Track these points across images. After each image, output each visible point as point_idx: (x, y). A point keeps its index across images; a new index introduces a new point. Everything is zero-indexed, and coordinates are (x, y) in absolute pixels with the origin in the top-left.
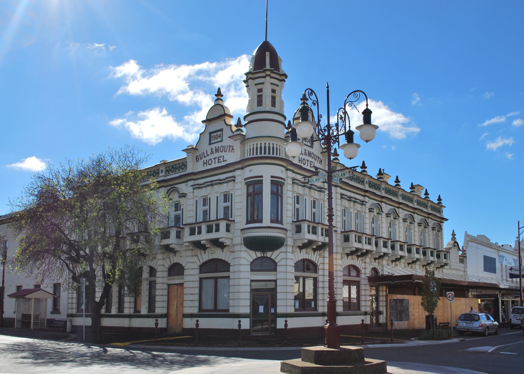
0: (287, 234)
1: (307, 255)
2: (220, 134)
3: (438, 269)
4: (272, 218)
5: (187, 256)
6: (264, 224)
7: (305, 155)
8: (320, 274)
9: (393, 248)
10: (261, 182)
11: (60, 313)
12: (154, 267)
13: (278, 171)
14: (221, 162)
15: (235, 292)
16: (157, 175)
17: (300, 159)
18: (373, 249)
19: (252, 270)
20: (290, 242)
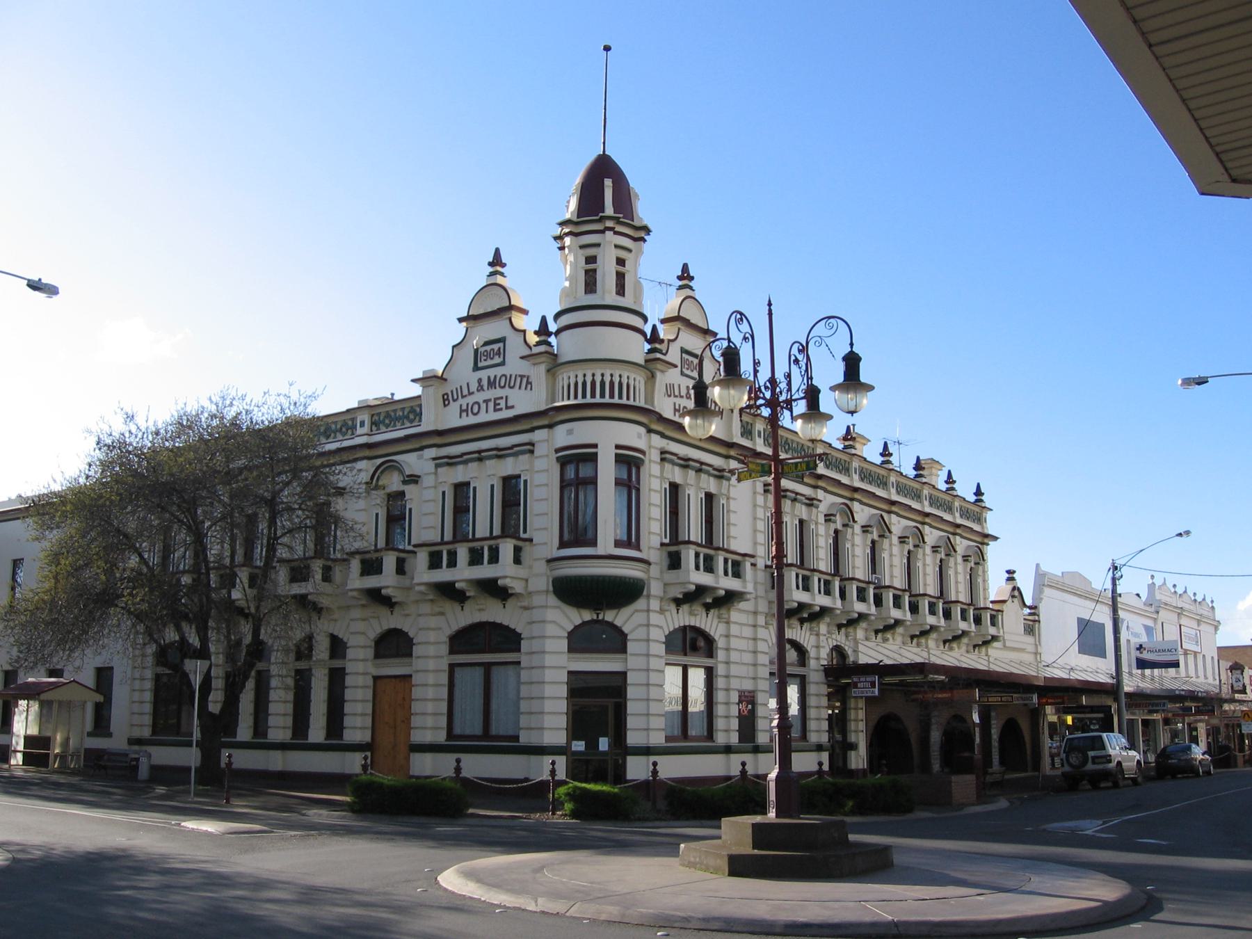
0: (648, 570)
1: (693, 618)
2: (499, 348)
3: (977, 650)
4: (618, 538)
5: (420, 615)
6: (601, 550)
7: (687, 398)
8: (719, 659)
9: (878, 601)
10: (593, 458)
11: (110, 735)
12: (340, 636)
13: (632, 435)
14: (501, 409)
15: (532, 698)
16: (350, 432)
17: (677, 407)
18: (835, 604)
19: (571, 650)
20: (655, 588)
